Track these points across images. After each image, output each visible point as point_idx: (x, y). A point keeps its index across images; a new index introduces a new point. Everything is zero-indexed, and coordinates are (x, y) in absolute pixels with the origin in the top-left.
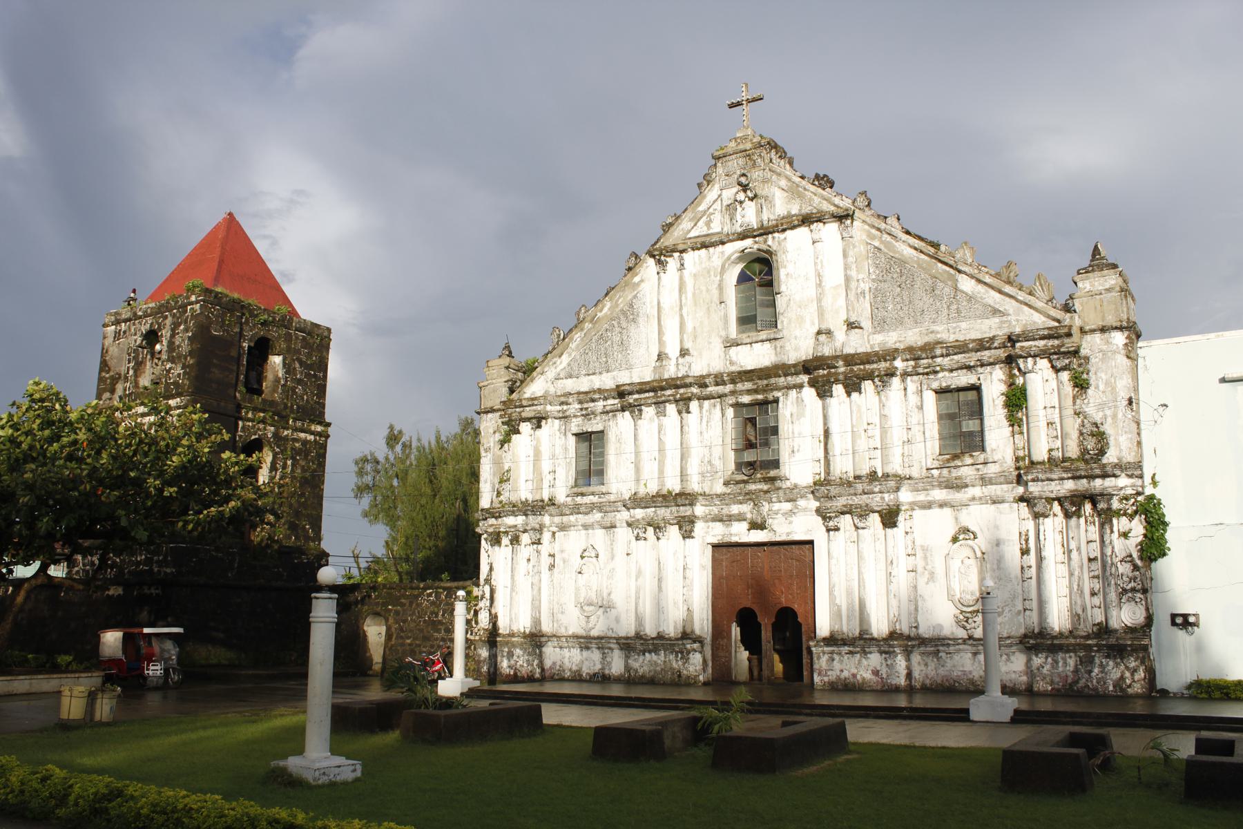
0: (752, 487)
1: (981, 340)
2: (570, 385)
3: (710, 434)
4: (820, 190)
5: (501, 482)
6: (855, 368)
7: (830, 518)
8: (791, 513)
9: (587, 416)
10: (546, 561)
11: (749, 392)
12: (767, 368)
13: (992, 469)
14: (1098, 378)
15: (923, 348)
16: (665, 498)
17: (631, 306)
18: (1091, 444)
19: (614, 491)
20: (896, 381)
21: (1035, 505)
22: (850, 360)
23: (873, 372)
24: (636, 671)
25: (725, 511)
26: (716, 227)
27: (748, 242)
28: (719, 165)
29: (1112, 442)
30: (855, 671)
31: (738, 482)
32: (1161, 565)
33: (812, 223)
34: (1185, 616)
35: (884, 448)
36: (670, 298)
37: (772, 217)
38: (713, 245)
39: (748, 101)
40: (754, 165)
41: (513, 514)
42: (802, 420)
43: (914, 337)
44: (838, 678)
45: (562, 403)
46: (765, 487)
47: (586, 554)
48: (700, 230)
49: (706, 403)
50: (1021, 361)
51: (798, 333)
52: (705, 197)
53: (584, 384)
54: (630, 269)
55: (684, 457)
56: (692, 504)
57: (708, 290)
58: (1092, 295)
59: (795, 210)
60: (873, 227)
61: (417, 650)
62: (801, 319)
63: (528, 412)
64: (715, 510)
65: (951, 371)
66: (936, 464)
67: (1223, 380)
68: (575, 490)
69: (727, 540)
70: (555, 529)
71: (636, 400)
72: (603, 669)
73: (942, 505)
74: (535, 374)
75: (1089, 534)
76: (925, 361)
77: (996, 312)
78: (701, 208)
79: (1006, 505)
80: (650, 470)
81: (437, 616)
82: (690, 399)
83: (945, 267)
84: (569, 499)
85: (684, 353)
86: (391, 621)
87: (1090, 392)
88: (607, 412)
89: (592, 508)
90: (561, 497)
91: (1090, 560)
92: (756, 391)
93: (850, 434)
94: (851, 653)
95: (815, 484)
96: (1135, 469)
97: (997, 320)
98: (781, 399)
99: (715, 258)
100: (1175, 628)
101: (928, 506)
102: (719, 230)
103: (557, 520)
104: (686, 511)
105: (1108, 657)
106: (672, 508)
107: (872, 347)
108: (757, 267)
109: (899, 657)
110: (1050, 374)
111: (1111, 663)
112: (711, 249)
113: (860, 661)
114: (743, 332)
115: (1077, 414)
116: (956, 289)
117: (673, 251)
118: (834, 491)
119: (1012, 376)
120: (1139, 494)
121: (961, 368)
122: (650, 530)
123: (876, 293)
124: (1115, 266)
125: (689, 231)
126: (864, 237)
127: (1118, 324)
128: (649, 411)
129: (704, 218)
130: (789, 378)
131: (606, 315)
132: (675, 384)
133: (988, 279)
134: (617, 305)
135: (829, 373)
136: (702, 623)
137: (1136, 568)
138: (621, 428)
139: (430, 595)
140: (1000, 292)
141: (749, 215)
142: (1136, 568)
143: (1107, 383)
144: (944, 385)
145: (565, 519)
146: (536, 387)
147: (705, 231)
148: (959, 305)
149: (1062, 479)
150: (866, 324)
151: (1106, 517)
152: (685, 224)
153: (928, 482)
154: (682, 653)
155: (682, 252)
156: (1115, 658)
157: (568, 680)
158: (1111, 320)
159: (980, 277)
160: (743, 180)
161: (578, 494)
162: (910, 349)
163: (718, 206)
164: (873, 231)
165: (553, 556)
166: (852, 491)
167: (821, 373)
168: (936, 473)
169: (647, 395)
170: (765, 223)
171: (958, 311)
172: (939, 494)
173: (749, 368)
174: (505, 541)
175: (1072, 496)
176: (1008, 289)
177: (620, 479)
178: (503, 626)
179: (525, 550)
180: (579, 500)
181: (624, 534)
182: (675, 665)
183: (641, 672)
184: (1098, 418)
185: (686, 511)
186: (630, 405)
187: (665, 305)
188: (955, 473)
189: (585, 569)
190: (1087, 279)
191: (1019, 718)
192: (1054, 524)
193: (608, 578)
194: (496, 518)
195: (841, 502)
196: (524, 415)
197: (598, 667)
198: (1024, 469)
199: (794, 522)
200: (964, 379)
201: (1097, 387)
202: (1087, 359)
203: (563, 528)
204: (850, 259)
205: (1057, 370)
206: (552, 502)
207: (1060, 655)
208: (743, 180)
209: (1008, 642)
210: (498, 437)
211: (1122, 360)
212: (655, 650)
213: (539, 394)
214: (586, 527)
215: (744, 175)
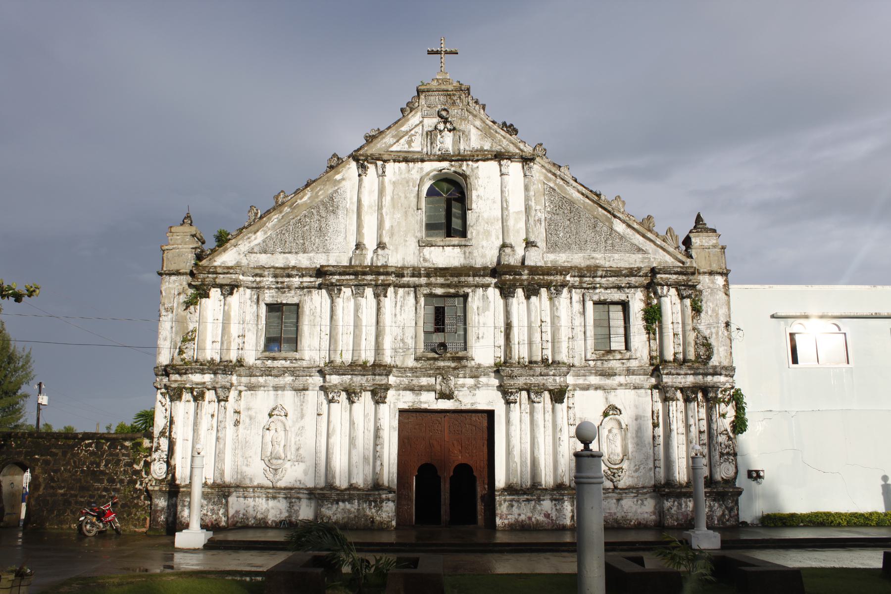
0: (441, 364)
1: (631, 268)
2: (264, 259)
3: (402, 319)
4: (508, 136)
5: (184, 340)
6: (536, 278)
7: (512, 393)
8: (476, 387)
9: (281, 289)
10: (231, 417)
11: (442, 286)
12: (455, 269)
13: (633, 364)
14: (707, 306)
15: (588, 268)
16: (355, 367)
17: (331, 199)
18: (702, 351)
19: (307, 357)
20: (565, 290)
21: (667, 392)
22: (534, 270)
23: (551, 282)
24: (330, 518)
25: (415, 382)
26: (416, 146)
27: (445, 164)
28: (422, 97)
29: (715, 351)
30: (530, 514)
31: (429, 359)
32: (741, 437)
33: (503, 159)
34: (757, 472)
35: (554, 341)
36: (369, 199)
37: (467, 148)
38: (414, 161)
39: (446, 53)
40: (454, 103)
41: (202, 372)
42: (487, 313)
43: (578, 259)
44: (517, 521)
45: (256, 275)
46: (453, 365)
47: (275, 412)
48: (401, 146)
49: (401, 291)
50: (659, 288)
51: (484, 243)
52: (408, 120)
53: (279, 260)
54: (332, 167)
55: (379, 335)
56: (387, 375)
57: (406, 197)
58: (703, 248)
59: (487, 147)
60: (550, 172)
61: (72, 500)
62: (487, 234)
63: (221, 279)
64: (406, 381)
65: (606, 288)
66: (594, 357)
67: (773, 317)
68: (267, 354)
69: (417, 406)
70: (242, 388)
71: (338, 280)
72: (290, 516)
74: (228, 245)
75: (700, 415)
76: (587, 279)
77: (639, 250)
78: (404, 128)
79: (642, 391)
80: (345, 343)
81: (98, 465)
82: (389, 285)
83: (604, 212)
84: (259, 362)
85: (381, 246)
86: (38, 470)
87: (702, 315)
88: (303, 288)
89: (284, 371)
90: (250, 358)
91: (700, 432)
92: (449, 286)
93: (526, 329)
94: (528, 500)
95: (496, 364)
96: (730, 371)
97: (640, 256)
98: (471, 294)
99: (414, 172)
101: (586, 388)
102: (419, 149)
103: (244, 380)
104: (380, 380)
105: (714, 500)
106: (366, 377)
107: (545, 262)
108: (445, 186)
109: (566, 503)
110: (676, 299)
111: (716, 505)
112: (411, 164)
113: (534, 507)
114: (431, 236)
115: (694, 329)
117: (378, 159)
118: (517, 371)
119: (648, 298)
120: (733, 388)
121: (614, 288)
122: (344, 395)
123: (550, 223)
124: (714, 231)
125: (392, 145)
126: (542, 178)
127: (721, 271)
128: (347, 292)
129: (406, 137)
130: (477, 279)
131: (305, 203)
132: (376, 271)
133: (635, 226)
134: (317, 197)
135: (514, 278)
137: (730, 438)
138: (316, 303)
139: (90, 445)
140: (644, 236)
141: (447, 142)
142: (730, 438)
143: (713, 310)
144: (602, 298)
145: (253, 380)
146: (227, 258)
147: (406, 148)
148: (614, 242)
149: (686, 374)
150: (542, 244)
151: (711, 402)
152: (388, 139)
153: (585, 370)
154: (375, 501)
155: (385, 161)
156: (719, 501)
157: (271, 528)
158: (715, 267)
159: (631, 223)
161: (269, 358)
162: (580, 269)
163: (419, 129)
164: (550, 175)
165: (239, 413)
166: (531, 373)
167: (508, 278)
168: (592, 363)
169: (348, 277)
170: (462, 152)
171: (613, 245)
172: (594, 380)
173: (440, 266)
174: (186, 396)
175: (694, 387)
176: (649, 235)
177: (313, 347)
178: (182, 474)
179: (209, 405)
180: (269, 363)
181: (314, 397)
182: (368, 512)
183: (334, 519)
184: (707, 333)
185: (380, 380)
186: (332, 284)
187: (365, 201)
188: (607, 365)
189: (273, 427)
190: (698, 236)
191: (210, 546)
192: (677, 407)
193: (297, 435)
194: (180, 374)
195: (521, 381)
196: (218, 281)
197: (285, 514)
198: (657, 366)
199: (483, 396)
200: (617, 296)
201: (707, 312)
202: (701, 292)
203: (251, 388)
204: (532, 193)
205: (682, 297)
206: (240, 363)
207: (683, 500)
208: (444, 113)
209: (645, 491)
210: (183, 298)
211: (721, 295)
212: (350, 500)
213: (231, 264)
214: (276, 388)
215: (445, 110)
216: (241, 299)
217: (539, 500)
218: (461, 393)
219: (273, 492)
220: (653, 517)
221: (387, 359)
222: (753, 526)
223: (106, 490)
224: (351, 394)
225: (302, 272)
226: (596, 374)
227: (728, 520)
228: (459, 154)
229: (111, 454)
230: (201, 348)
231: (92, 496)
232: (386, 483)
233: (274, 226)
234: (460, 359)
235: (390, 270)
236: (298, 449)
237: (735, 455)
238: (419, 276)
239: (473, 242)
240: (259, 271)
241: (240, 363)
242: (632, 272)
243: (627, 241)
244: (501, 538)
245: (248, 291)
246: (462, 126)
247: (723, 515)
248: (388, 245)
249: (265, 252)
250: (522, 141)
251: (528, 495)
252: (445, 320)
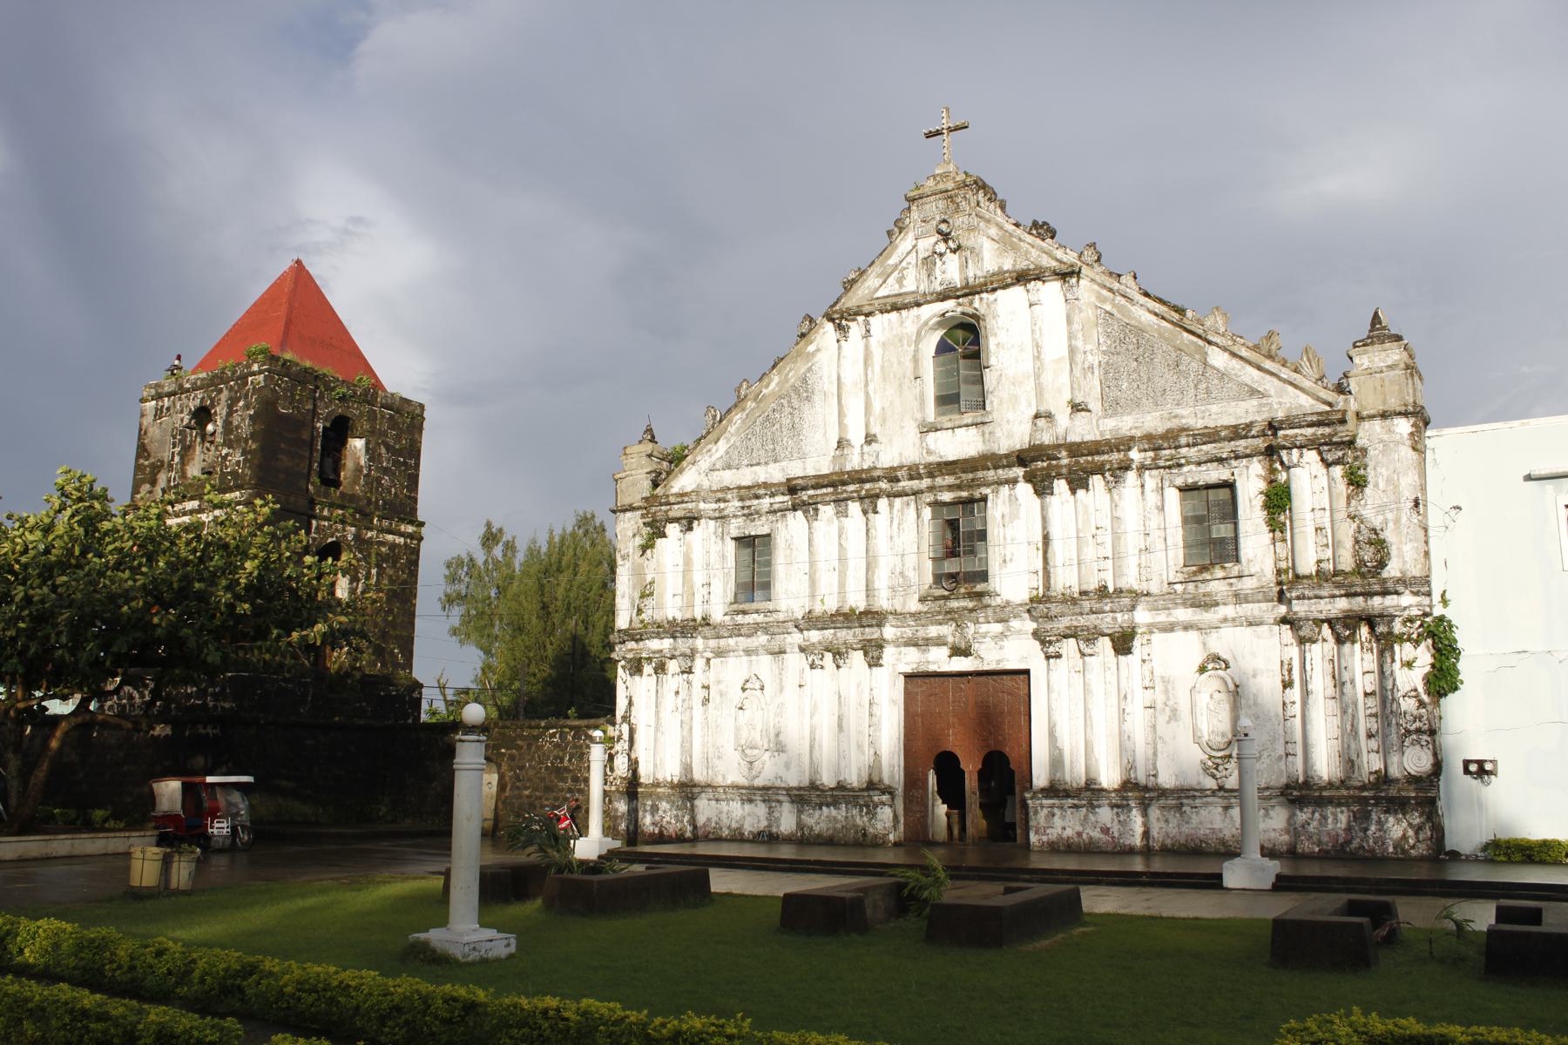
0: (954, 604)
2: (729, 478)
3: (902, 540)
4: (1038, 241)
6: (1082, 460)
7: (1050, 642)
9: (750, 515)
10: (698, 694)
11: (950, 488)
13: (1248, 584)
14: (1377, 474)
16: (846, 618)
17: (805, 381)
18: (1368, 554)
19: (783, 608)
20: (1131, 476)
21: (1300, 628)
22: (1075, 449)
25: (921, 633)
26: (910, 285)
29: (1394, 552)
30: (1079, 829)
31: (937, 599)
32: (1451, 703)
34: (1480, 763)
35: (1116, 557)
37: (979, 274)
38: (906, 307)
39: (950, 130)
41: (659, 636)
45: (719, 500)
46: (971, 605)
48: (890, 288)
49: (898, 502)
50: (1284, 453)
51: (1011, 416)
53: (746, 477)
54: (803, 335)
55: (870, 567)
56: (880, 625)
57: (899, 363)
58: (1370, 372)
59: (1008, 265)
60: (1104, 287)
62: (1015, 400)
63: (676, 511)
64: (908, 632)
65: (1199, 464)
66: (1180, 577)
67: (1528, 478)
68: (735, 607)
69: (923, 668)
70: (710, 655)
71: (811, 497)
72: (769, 826)
73: (1187, 627)
74: (684, 463)
76: (1167, 452)
77: (1253, 392)
78: (892, 261)
79: (1265, 628)
81: (562, 761)
82: (878, 496)
83: (1192, 337)
84: (727, 618)
85: (870, 439)
86: (504, 767)
87: (1368, 491)
88: (775, 512)
90: (717, 616)
92: (959, 487)
94: (1075, 806)
95: (1031, 600)
96: (1421, 585)
97: (1255, 402)
99: (908, 323)
101: (1169, 628)
103: (713, 643)
104: (872, 633)
106: (855, 629)
107: (1102, 434)
108: (960, 334)
109: (1134, 812)
110: (1319, 468)
112: (904, 312)
118: (1055, 609)
119: (1273, 471)
121: (1211, 461)
122: (828, 656)
123: (1107, 368)
124: (1398, 338)
125: (877, 290)
126: (1093, 299)
127: (1403, 409)
128: (827, 511)
129: (895, 274)
130: (1000, 471)
131: (773, 392)
132: (859, 477)
133: (1244, 353)
134: (787, 380)
136: (892, 764)
137: (1422, 704)
139: (553, 735)
140: (1259, 368)
141: (951, 271)
142: (1422, 704)
143: (1388, 481)
144: (1190, 481)
145: (722, 642)
146: (686, 480)
147: (896, 289)
148: (1209, 383)
149: (1333, 596)
150: (1095, 406)
152: (872, 281)
153: (1170, 599)
154: (868, 806)
155: (868, 315)
156: (1396, 812)
157: (748, 841)
158: (1394, 404)
159: (1235, 349)
161: (738, 612)
162: (1149, 437)
163: (912, 258)
164: (1104, 292)
165: (708, 688)
166: (1077, 610)
167: (1040, 466)
168: (1179, 588)
169: (824, 490)
170: (971, 281)
171: (1208, 391)
172: (1183, 614)
173: (951, 458)
174: (648, 669)
176: (1268, 365)
177: (791, 592)
179: (672, 680)
180: (739, 619)
181: (795, 661)
182: (859, 821)
183: (817, 830)
184: (1377, 522)
185: (872, 633)
186: (804, 503)
187: (847, 380)
188: (1203, 588)
189: (747, 704)
194: (637, 641)
195: (1063, 624)
196: (671, 514)
198: (1287, 584)
199: (1005, 647)
200: (1215, 474)
201: (1377, 485)
202: (1364, 451)
203: (720, 653)
204: (1076, 326)
205: (1328, 465)
206: (706, 621)
207: (1330, 810)
208: (943, 227)
210: (639, 541)
211: (1407, 453)
212: (835, 803)
214: (748, 652)
215: (944, 221)
216: (704, 530)
217: (1092, 807)
218: (983, 646)
219: (750, 793)
220: (1286, 838)
221: (883, 602)
222: (1472, 860)
223: (570, 790)
224: (838, 654)
225: (770, 488)
226: (1184, 604)
227: (1413, 847)
228: (967, 286)
229: (575, 746)
230: (660, 606)
231: (556, 799)
232: (886, 781)
233: (738, 430)
234: (980, 595)
235: (876, 474)
236: (777, 735)
237: (1432, 732)
238: (920, 477)
239: (995, 415)
240: (721, 494)
241: (706, 621)
242: (1237, 433)
243: (1230, 379)
244: (1038, 862)
245: (712, 523)
246: (968, 241)
247: (1404, 837)
248: (879, 437)
249: (729, 467)
250: (1061, 246)
251: (1073, 798)
252: (960, 539)
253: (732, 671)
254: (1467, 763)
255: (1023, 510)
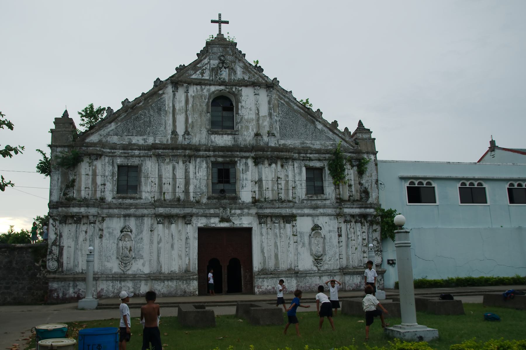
12: (229, 147)
26: (206, 76)
27: (222, 88)
36: (180, 104)
51: (245, 133)
57: (200, 105)
62: (247, 128)
73: (308, 215)
85: (187, 133)
90: (109, 197)
100: (389, 265)
116: (316, 127)
136: (194, 265)
138: (150, 166)
150: (278, 135)
160: (222, 58)
177: (148, 191)
187: (177, 107)
208: (222, 58)
215: (223, 56)
218: (233, 218)
230: (79, 191)
252: (224, 176)
253: (115, 225)
254: (388, 261)
255: (250, 168)
